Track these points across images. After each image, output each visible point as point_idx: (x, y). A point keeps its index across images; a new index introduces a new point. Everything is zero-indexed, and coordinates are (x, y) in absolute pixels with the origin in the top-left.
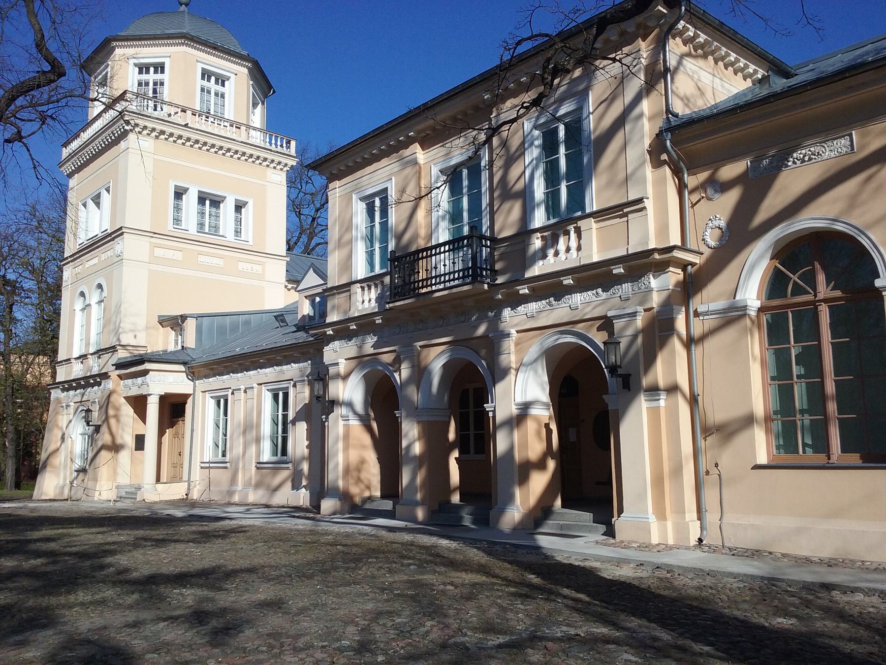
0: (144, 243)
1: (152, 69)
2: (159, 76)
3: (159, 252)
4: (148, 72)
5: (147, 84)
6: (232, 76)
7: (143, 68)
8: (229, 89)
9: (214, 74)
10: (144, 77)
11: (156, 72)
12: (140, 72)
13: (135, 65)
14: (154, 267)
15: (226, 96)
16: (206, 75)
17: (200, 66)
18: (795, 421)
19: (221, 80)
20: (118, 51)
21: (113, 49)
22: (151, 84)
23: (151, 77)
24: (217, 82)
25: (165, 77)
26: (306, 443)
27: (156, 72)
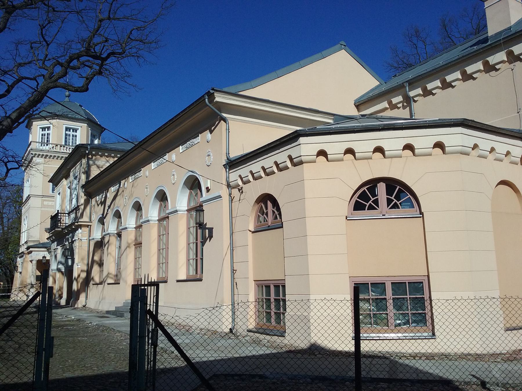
0: (39, 200)
1: (71, 130)
2: (74, 134)
3: (46, 203)
4: (45, 130)
5: (45, 135)
6: (80, 128)
7: (43, 129)
8: (78, 134)
9: (46, 127)
10: (43, 132)
11: (48, 130)
12: (42, 131)
13: (41, 128)
14: (43, 209)
15: (77, 136)
16: (67, 129)
17: (64, 126)
18: (270, 312)
19: (75, 130)
20: (34, 123)
21: (32, 122)
22: (71, 136)
23: (46, 132)
24: (73, 131)
25: (50, 132)
26: (207, 135)
27: (48, 130)
